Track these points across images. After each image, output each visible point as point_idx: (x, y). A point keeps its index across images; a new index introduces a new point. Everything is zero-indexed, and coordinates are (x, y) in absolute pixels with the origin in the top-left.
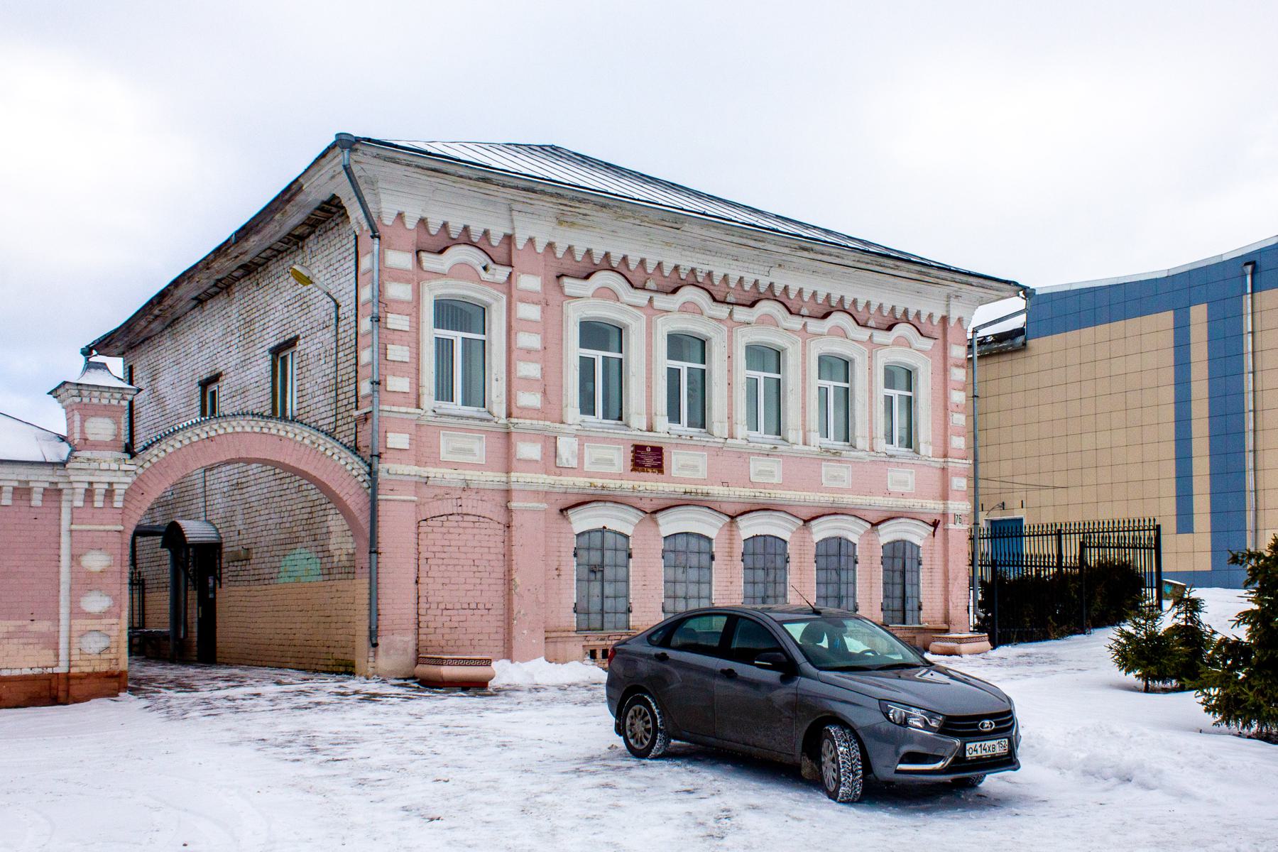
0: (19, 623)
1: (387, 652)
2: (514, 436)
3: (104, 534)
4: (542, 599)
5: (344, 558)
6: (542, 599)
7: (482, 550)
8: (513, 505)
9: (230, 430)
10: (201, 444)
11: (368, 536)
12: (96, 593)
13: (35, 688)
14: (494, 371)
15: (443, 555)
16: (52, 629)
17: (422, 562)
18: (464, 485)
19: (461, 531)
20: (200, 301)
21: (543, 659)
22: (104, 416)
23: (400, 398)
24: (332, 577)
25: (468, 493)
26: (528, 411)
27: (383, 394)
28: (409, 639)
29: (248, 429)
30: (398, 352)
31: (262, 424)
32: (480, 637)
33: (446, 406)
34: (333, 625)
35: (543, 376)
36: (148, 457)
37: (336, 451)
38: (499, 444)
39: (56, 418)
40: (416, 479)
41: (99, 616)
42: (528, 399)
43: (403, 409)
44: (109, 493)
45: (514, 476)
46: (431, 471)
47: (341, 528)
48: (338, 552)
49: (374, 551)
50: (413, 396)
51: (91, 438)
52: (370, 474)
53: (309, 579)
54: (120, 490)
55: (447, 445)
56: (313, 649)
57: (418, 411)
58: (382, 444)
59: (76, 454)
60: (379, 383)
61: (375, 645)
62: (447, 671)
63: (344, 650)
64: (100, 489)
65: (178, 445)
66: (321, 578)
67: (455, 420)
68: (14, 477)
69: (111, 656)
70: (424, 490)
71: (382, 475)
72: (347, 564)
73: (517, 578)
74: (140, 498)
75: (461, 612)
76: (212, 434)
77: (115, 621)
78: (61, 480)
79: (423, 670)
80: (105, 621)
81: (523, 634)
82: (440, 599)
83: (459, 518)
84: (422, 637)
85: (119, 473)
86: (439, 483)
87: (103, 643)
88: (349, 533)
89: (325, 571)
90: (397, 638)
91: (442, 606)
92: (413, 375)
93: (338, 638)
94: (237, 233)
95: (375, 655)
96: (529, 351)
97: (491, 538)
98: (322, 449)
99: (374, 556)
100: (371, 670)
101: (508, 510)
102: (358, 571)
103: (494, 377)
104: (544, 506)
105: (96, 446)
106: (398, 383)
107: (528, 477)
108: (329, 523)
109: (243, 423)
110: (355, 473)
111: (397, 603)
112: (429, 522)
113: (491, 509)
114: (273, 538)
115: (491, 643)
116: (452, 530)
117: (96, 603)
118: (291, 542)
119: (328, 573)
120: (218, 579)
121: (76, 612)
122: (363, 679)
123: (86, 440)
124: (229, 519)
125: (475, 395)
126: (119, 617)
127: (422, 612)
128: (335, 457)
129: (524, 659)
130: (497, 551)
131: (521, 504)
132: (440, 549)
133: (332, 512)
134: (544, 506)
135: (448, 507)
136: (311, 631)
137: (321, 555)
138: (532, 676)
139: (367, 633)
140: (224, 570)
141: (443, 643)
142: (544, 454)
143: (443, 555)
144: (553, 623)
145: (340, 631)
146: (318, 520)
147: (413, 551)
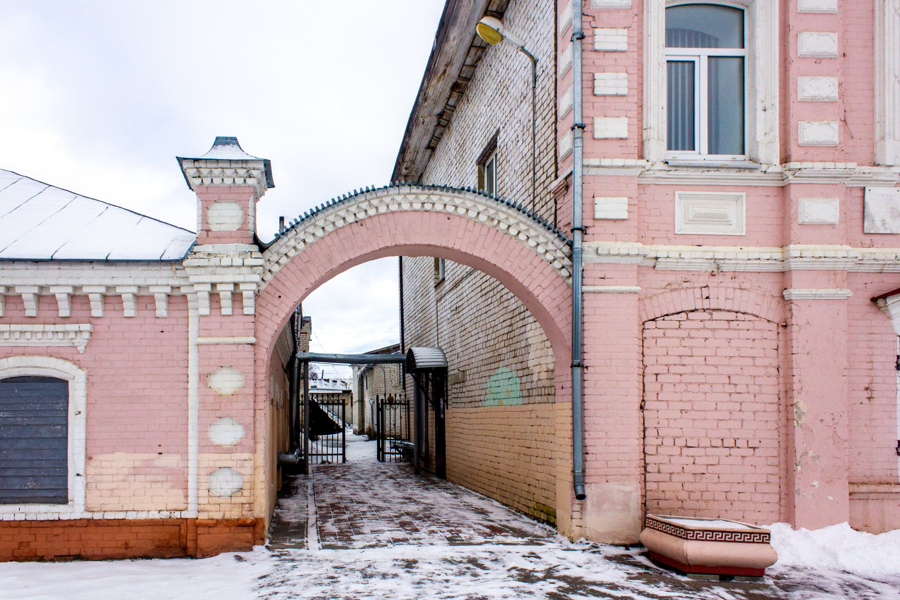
0: (146, 456)
1: (599, 505)
2: (794, 192)
3: (234, 348)
4: (843, 433)
5: (544, 376)
6: (843, 433)
7: (743, 362)
8: (794, 292)
9: (383, 209)
10: (348, 230)
11: (569, 343)
12: (227, 421)
13: (162, 535)
14: (760, 96)
15: (681, 370)
16: (181, 464)
17: (650, 379)
18: (713, 268)
19: (708, 334)
20: (432, 148)
21: (846, 525)
22: (230, 201)
23: (614, 147)
24: (532, 400)
25: (720, 278)
26: (815, 149)
27: (589, 142)
28: (632, 490)
29: (406, 206)
30: (610, 82)
31: (423, 198)
32: (740, 488)
33: (683, 156)
34: (534, 459)
35: (842, 95)
36: (284, 250)
37: (523, 227)
38: (768, 205)
39: (186, 211)
40: (639, 260)
41: (230, 450)
42: (816, 132)
43: (619, 162)
44: (237, 296)
45: (794, 249)
46: (661, 250)
47: (540, 339)
48: (537, 370)
49: (578, 364)
50: (633, 143)
51: (214, 228)
52: (570, 257)
53: (510, 402)
54: (248, 291)
55: (686, 211)
56: (516, 485)
57: (642, 162)
58: (587, 215)
59: (196, 249)
60: (582, 127)
61: (582, 497)
62: (694, 550)
63: (546, 494)
64: (225, 291)
65: (320, 233)
66: (521, 401)
67: (697, 173)
68: (131, 282)
69: (244, 500)
70: (651, 276)
71: (589, 257)
72: (546, 383)
73: (802, 403)
74: (277, 302)
75: (711, 451)
76: (361, 216)
77: (246, 456)
78: (182, 282)
79: (650, 536)
80: (236, 456)
81: (808, 486)
82: (678, 433)
83: (706, 316)
84: (650, 486)
85: (244, 270)
86: (671, 266)
87: (236, 483)
88: (548, 344)
89: (525, 393)
90: (613, 486)
91: (680, 442)
92: (634, 114)
93: (538, 476)
94: (437, 37)
95: (582, 509)
96: (818, 60)
97: (761, 343)
98: (503, 226)
99: (578, 370)
100: (576, 530)
101: (785, 302)
102: (559, 392)
103: (759, 106)
104: (847, 292)
105: (221, 238)
106: (611, 127)
107: (818, 250)
108: (529, 335)
109: (399, 198)
110: (549, 257)
111: (613, 437)
112: (660, 323)
113: (759, 301)
114: (481, 358)
115: (758, 497)
116: (693, 333)
117: (227, 433)
118: (496, 360)
119: (527, 395)
120: (446, 401)
121: (206, 446)
122: (566, 543)
123: (208, 231)
124: (451, 344)
125: (729, 134)
126: (254, 451)
127: (650, 450)
128: (522, 237)
129: (817, 524)
130: (766, 362)
131: (806, 291)
132: (677, 360)
133: (531, 319)
134: (847, 292)
135: (688, 300)
136: (512, 463)
137: (521, 373)
138: (834, 556)
139: (570, 478)
140: (450, 393)
141: (683, 495)
142: (845, 214)
143: (681, 370)
144: (861, 470)
145: (541, 468)
146: (517, 332)
147: (637, 364)
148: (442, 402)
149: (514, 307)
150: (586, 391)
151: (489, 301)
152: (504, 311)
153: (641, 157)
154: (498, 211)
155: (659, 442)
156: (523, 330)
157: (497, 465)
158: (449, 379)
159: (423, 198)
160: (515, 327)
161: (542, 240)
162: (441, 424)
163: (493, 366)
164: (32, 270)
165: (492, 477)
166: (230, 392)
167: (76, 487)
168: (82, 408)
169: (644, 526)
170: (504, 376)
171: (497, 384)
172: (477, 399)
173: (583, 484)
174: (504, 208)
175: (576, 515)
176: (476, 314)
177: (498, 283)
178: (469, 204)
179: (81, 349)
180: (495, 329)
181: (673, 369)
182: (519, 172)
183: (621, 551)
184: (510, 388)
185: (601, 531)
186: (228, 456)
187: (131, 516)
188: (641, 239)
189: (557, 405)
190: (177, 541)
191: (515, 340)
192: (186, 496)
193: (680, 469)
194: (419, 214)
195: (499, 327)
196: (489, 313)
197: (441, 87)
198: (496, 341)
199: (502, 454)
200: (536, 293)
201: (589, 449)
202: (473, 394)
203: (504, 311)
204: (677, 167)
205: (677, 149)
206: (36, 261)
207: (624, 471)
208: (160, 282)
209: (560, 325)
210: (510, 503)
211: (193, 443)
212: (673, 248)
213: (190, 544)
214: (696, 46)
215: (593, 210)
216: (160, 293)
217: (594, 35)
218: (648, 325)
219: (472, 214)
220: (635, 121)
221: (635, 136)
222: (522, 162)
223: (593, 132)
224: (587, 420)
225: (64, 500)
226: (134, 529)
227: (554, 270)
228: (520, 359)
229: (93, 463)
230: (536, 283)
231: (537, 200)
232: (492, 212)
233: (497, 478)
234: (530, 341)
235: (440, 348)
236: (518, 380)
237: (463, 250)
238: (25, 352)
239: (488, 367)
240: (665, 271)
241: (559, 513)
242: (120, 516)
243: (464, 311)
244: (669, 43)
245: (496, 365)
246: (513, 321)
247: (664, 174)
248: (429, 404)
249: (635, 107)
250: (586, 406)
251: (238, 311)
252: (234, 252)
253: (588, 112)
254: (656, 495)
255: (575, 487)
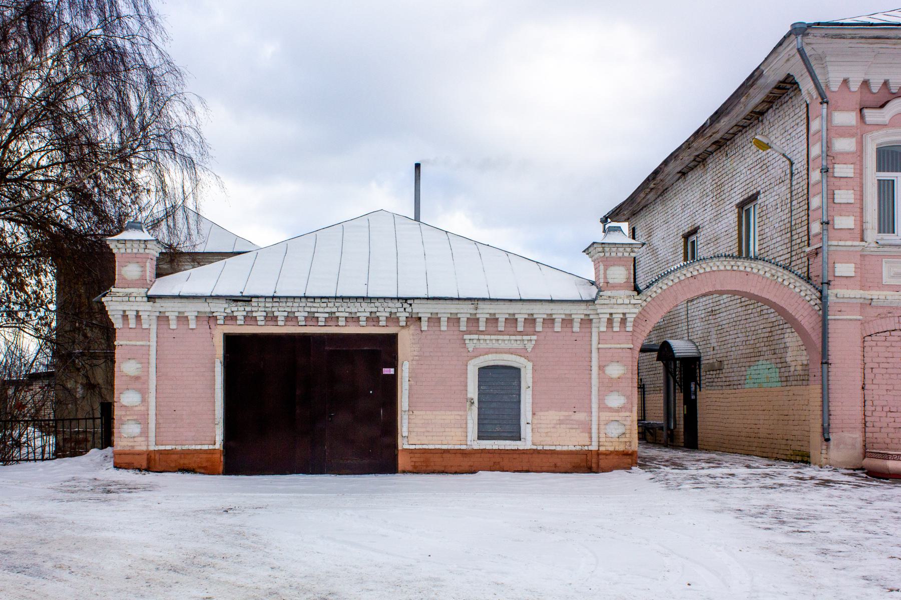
0: (567, 413)
1: (837, 445)
5: (799, 368)
9: (708, 269)
12: (616, 393)
13: (577, 460)
15: (886, 365)
16: (587, 419)
17: (868, 371)
20: (683, 174)
22: (619, 265)
24: (789, 383)
28: (858, 436)
29: (722, 268)
30: (844, 196)
31: (732, 263)
33: (888, 238)
34: (790, 422)
36: (649, 294)
37: (792, 281)
40: (862, 301)
43: (849, 243)
44: (624, 321)
46: (874, 294)
48: (793, 364)
49: (825, 362)
50: (858, 231)
51: (611, 281)
52: (820, 299)
54: (630, 318)
56: (775, 441)
57: (863, 243)
58: (831, 273)
59: (601, 293)
60: (828, 223)
61: (828, 440)
64: (617, 318)
67: (896, 249)
71: (831, 299)
72: (802, 373)
74: (644, 323)
76: (695, 273)
77: (628, 414)
78: (591, 312)
79: (870, 462)
82: (885, 403)
84: (867, 435)
86: (881, 304)
87: (621, 430)
88: (803, 348)
93: (794, 433)
95: (828, 448)
98: (780, 280)
99: (825, 366)
100: (824, 461)
105: (614, 287)
106: (845, 222)
108: (786, 340)
110: (808, 298)
111: (846, 406)
112: (874, 338)
114: (740, 352)
117: (615, 400)
119: (786, 380)
121: (603, 407)
122: (817, 467)
127: (868, 413)
128: (791, 286)
132: (884, 360)
136: (772, 427)
137: (780, 366)
139: (820, 430)
141: (888, 440)
143: (886, 365)
145: (797, 428)
146: (776, 337)
148: (693, 386)
149: (774, 319)
150: (830, 378)
151: (750, 311)
152: (764, 321)
153: (862, 240)
154: (777, 271)
155: (873, 408)
156: (782, 336)
157: (756, 431)
158: (702, 366)
159: (732, 263)
160: (774, 333)
161: (803, 288)
162: (691, 405)
163: (753, 359)
164: (508, 304)
165: (752, 439)
166: (617, 376)
167: (526, 430)
168: (530, 385)
169: (865, 457)
170: (764, 367)
171: (758, 372)
172: (736, 383)
173: (829, 433)
174: (781, 270)
175: (824, 452)
176: (736, 319)
177: (785, 321)
178: (760, 267)
179: (529, 350)
180: (755, 333)
181: (882, 365)
182: (779, 229)
183: (852, 472)
184: (770, 375)
185: (839, 460)
186: (616, 414)
187: (559, 448)
188: (862, 288)
189: (810, 387)
190: (587, 463)
191: (774, 342)
192: (591, 438)
193: (885, 425)
194: (729, 273)
195: (760, 331)
196: (749, 321)
197: (704, 143)
198: (756, 341)
199: (761, 422)
200: (800, 319)
201: (832, 413)
202: (731, 379)
203: (764, 321)
204: (884, 246)
205: (884, 232)
206: (511, 300)
207: (852, 426)
208: (578, 312)
209: (814, 339)
210: (769, 455)
211: (595, 406)
212: (881, 293)
213: (594, 465)
214: (897, 171)
215: (834, 272)
216: (577, 318)
217: (834, 168)
218: (866, 339)
219: (761, 272)
220: (858, 218)
221: (859, 227)
222: (781, 223)
223: (833, 224)
224: (831, 395)
225: (519, 438)
226: (560, 456)
227: (810, 306)
228: (780, 356)
229: (536, 417)
230: (800, 313)
231: (794, 253)
232: (773, 272)
233: (756, 440)
234: (788, 344)
235: (691, 341)
236: (777, 370)
237: (756, 293)
238: (497, 351)
239: (749, 360)
240: (877, 307)
241: (812, 452)
242: (553, 448)
243: (721, 315)
244: (879, 169)
245: (756, 359)
246: (773, 329)
247: (876, 249)
248: (677, 387)
249: (859, 210)
250: (830, 387)
251: (623, 329)
252: (624, 295)
253: (831, 213)
254: (872, 440)
255: (823, 434)
